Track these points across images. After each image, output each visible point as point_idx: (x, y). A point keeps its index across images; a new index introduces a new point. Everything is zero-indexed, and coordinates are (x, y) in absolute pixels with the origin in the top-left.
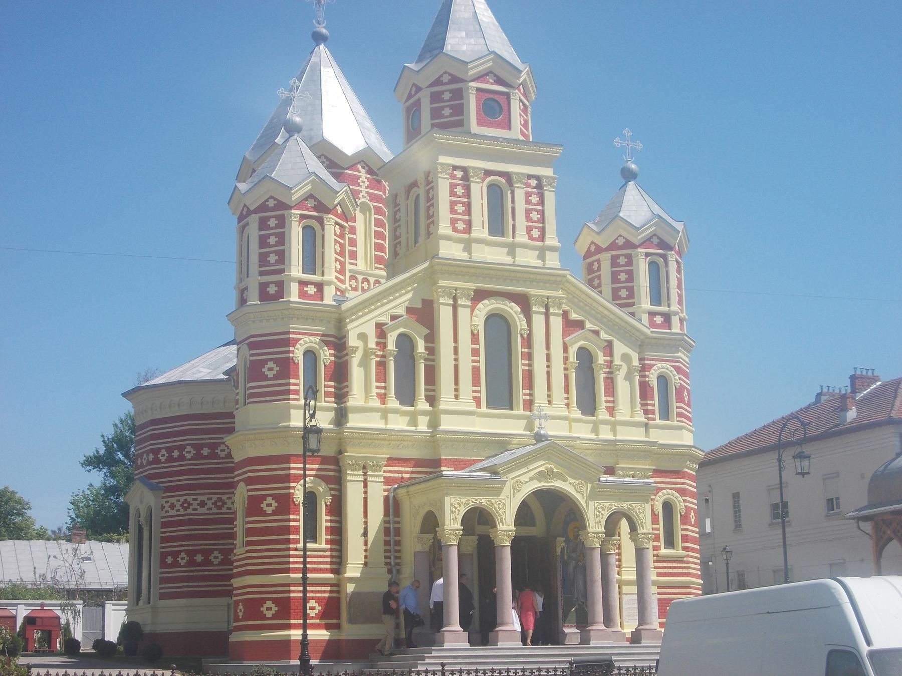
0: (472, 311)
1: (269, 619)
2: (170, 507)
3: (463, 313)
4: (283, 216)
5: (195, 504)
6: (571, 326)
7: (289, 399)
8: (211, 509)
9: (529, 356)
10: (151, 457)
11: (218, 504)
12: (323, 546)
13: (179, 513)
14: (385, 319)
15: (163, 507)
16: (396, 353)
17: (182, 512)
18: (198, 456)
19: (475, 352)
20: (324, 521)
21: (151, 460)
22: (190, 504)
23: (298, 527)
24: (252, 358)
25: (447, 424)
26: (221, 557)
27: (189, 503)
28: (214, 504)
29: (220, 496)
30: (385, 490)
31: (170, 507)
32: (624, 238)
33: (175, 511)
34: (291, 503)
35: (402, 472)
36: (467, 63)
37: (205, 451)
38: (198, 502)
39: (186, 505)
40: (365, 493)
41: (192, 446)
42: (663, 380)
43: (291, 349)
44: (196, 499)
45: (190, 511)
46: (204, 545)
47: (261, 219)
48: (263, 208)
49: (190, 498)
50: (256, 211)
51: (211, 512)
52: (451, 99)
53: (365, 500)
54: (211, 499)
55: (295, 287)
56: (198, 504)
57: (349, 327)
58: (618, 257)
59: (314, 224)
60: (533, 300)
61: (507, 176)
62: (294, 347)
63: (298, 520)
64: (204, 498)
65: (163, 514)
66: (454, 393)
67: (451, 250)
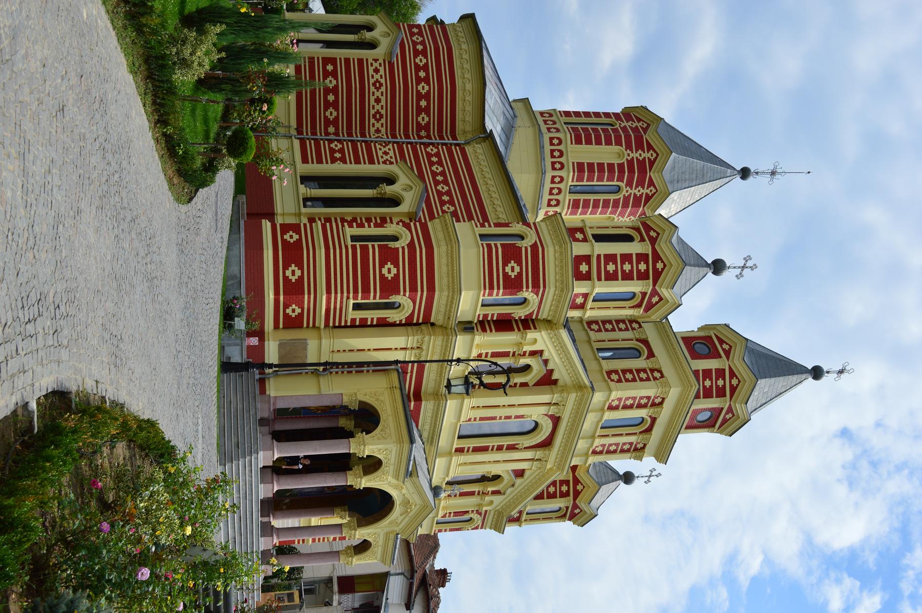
0: (546, 415)
1: (284, 273)
2: (377, 74)
3: (543, 410)
4: (648, 278)
5: (378, 94)
6: (520, 474)
7: (485, 289)
9: (500, 448)
10: (420, 47)
12: (350, 317)
13: (380, 158)
15: (376, 60)
17: (372, 81)
18: (420, 96)
20: (372, 315)
22: (378, 89)
26: (331, 109)
27: (380, 88)
31: (377, 74)
32: (582, 490)
33: (373, 73)
36: (746, 404)
37: (423, 103)
38: (375, 74)
44: (382, 95)
47: (647, 255)
48: (657, 257)
49: (383, 89)
50: (654, 250)
51: (371, 108)
52: (711, 379)
54: (382, 108)
55: (584, 290)
57: (543, 333)
60: (547, 452)
61: (649, 430)
63: (375, 298)
64: (383, 102)
65: (370, 61)
66: (476, 406)
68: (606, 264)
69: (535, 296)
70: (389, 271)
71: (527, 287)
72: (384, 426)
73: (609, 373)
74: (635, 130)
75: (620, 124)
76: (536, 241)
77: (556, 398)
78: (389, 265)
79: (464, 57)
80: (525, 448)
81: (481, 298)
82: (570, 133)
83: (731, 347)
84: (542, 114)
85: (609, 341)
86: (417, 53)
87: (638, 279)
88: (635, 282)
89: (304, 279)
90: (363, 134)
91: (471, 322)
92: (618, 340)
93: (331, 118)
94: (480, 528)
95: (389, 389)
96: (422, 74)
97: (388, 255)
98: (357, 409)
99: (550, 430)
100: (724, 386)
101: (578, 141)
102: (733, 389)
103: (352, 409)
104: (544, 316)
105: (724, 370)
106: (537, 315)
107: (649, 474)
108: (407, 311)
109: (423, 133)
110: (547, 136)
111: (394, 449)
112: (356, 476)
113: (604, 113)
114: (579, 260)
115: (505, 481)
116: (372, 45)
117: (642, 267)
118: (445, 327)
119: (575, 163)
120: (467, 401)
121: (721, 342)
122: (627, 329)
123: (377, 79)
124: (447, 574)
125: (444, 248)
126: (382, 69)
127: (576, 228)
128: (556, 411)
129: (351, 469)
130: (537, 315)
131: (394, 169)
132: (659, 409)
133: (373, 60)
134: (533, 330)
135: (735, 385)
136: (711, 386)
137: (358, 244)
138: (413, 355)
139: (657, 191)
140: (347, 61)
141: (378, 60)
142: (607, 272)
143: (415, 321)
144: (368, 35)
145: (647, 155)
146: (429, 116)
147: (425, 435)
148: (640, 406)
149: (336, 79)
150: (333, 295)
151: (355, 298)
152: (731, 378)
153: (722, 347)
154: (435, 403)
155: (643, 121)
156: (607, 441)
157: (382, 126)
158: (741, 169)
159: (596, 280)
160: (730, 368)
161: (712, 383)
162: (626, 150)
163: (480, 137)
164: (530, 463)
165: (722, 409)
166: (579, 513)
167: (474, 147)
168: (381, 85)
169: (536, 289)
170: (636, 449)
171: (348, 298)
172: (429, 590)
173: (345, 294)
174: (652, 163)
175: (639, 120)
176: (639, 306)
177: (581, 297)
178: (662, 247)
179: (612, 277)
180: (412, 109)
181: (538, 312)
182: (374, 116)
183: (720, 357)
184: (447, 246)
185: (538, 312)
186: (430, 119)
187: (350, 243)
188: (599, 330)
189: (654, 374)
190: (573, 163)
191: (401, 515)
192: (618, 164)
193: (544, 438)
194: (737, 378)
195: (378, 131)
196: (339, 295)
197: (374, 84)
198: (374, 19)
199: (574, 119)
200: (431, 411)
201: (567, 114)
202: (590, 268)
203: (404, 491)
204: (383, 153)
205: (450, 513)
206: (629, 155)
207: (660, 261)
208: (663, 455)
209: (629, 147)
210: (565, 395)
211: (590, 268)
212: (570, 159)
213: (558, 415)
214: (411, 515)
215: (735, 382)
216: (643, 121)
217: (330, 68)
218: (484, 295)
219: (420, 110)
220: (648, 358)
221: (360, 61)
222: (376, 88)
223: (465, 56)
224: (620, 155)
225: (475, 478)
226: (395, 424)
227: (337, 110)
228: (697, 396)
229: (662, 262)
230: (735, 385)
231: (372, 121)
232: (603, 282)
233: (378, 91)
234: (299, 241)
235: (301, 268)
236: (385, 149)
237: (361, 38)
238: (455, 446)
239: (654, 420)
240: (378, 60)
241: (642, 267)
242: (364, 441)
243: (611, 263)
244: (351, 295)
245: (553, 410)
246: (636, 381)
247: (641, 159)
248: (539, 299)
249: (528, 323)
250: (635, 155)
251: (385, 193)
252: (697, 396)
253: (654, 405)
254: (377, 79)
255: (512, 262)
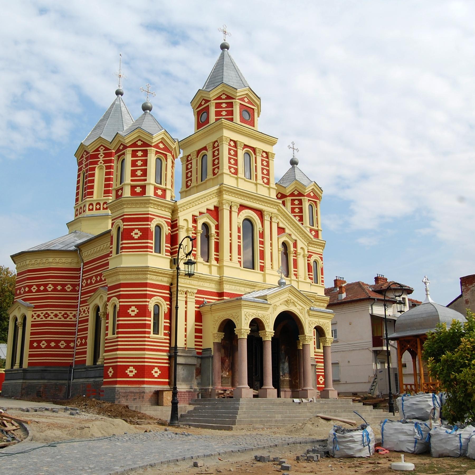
1: (156, 378)
2: (40, 316)
3: (234, 215)
5: (52, 315)
6: (281, 230)
8: (61, 318)
9: (262, 243)
10: (27, 289)
11: (65, 316)
14: (197, 214)
15: (33, 316)
16: (202, 232)
17: (44, 319)
19: (239, 238)
20: (163, 322)
21: (27, 291)
22: (49, 315)
23: (150, 324)
24: (125, 227)
25: (228, 273)
28: (63, 316)
29: (66, 312)
30: (196, 307)
32: (298, 191)
33: (40, 318)
34: (147, 310)
35: (203, 298)
37: (59, 288)
39: (47, 315)
40: (186, 308)
41: (52, 284)
42: (315, 262)
43: (149, 223)
44: (53, 313)
45: (49, 319)
46: (56, 338)
49: (49, 312)
50: (130, 146)
51: (60, 320)
52: (222, 111)
53: (186, 312)
56: (54, 316)
58: (294, 200)
59: (163, 157)
60: (265, 213)
61: (254, 149)
62: (151, 222)
64: (57, 312)
67: (229, 181)
68: (136, 176)
69: (154, 220)
70: (133, 311)
71: (148, 225)
72: (232, 317)
73: (214, 174)
74: (87, 159)
75: (84, 168)
76: (121, 219)
77: (226, 208)
78: (129, 311)
79: (39, 262)
80: (263, 227)
81: (154, 253)
82: (87, 198)
83: (203, 99)
84: (76, 215)
85: (197, 174)
86: (30, 291)
87: (147, 156)
88: (148, 158)
89: (135, 365)
90: (75, 325)
91: (171, 261)
92: (197, 168)
93: (65, 344)
94: (321, 256)
95: (212, 313)
96: (59, 288)
97: (123, 311)
98: (224, 333)
99: (250, 211)
100: (226, 103)
101: (92, 193)
102: (228, 97)
103: (223, 336)
104: (170, 214)
105: (216, 103)
106: (169, 219)
107: (292, 150)
108: (160, 300)
109: (77, 288)
110: (88, 213)
111: (245, 310)
112: (265, 335)
113: (78, 178)
114: (133, 193)
115: (287, 239)
116: (25, 318)
117: (140, 154)
118: (173, 276)
119: (104, 195)
120: (225, 263)
121: (200, 105)
122: (191, 163)
123: (43, 316)
124: (378, 277)
125: (121, 277)
126: (38, 313)
127: (116, 195)
128: (235, 207)
129: (261, 338)
130: (169, 219)
131: (91, 306)
132: (238, 143)
133: (32, 318)
134: (178, 221)
135: (226, 96)
136: (226, 111)
137: (116, 330)
138: (191, 297)
139: (102, 145)
140: (32, 334)
141: (32, 315)
142: (142, 176)
143: (168, 296)
144: (20, 320)
145: (102, 152)
146: (67, 284)
147: (248, 290)
148: (236, 155)
149: (42, 341)
150: (146, 347)
151: (149, 333)
152: (221, 99)
153: (203, 105)
154: (226, 284)
155: (83, 154)
156: (260, 175)
157: (72, 313)
158: (117, 95)
159: (146, 182)
160: (215, 100)
161: (224, 111)
162: (98, 164)
163: (80, 253)
164: (273, 224)
165: (240, 104)
166: (313, 193)
167: (84, 257)
168: (47, 313)
169: (149, 219)
170: (267, 157)
171: (149, 337)
172: (385, 288)
173: (146, 339)
174: (106, 149)
175: (82, 157)
176: (166, 156)
177: (157, 191)
178: (128, 141)
179: (145, 173)
180: (62, 294)
181: (166, 218)
182: (65, 318)
183: (208, 106)
184: (119, 274)
185: (166, 218)
186: (69, 284)
187: (116, 336)
188: (191, 180)
189: (216, 146)
190: (104, 196)
191: (296, 306)
192: (106, 169)
193: (255, 215)
194: (221, 95)
195: (74, 316)
196: (146, 343)
197: (46, 318)
198: (11, 317)
199: (80, 196)
200: (231, 286)
201: (77, 200)
202: (138, 186)
203: (278, 304)
204: (84, 313)
205: (309, 275)
206: (101, 163)
207: (137, 143)
208: (271, 142)
209: (96, 163)
210: (224, 201)
211: (138, 186)
212: (101, 199)
213: (239, 206)
214: (296, 300)
215: (224, 97)
216: (83, 154)
217: (35, 345)
218: (152, 252)
219: (63, 290)
220: (207, 150)
221: (33, 326)
222: (48, 317)
223: (33, 261)
224: (101, 168)
225: (285, 258)
226: (230, 309)
227: (60, 341)
228: (232, 120)
229: (137, 141)
230: (226, 96)
231: (68, 319)
232: (147, 178)
233: (62, 316)
234: (113, 367)
235: (128, 367)
236: (86, 311)
237: (21, 325)
238: (259, 271)
239: (246, 146)
240: (32, 315)
241: (140, 154)
242: (239, 330)
243: (136, 173)
244: (147, 335)
245: (235, 209)
246: (219, 158)
247: (99, 156)
248: (156, 217)
249: (174, 225)
250: (101, 159)
251: (103, 312)
252: (232, 120)
253: (236, 146)
254: (43, 316)
255: (132, 234)
